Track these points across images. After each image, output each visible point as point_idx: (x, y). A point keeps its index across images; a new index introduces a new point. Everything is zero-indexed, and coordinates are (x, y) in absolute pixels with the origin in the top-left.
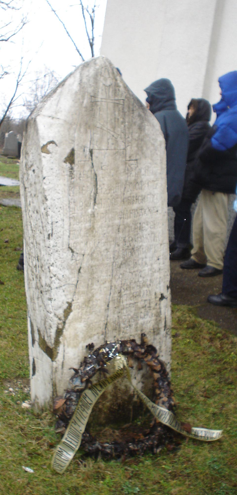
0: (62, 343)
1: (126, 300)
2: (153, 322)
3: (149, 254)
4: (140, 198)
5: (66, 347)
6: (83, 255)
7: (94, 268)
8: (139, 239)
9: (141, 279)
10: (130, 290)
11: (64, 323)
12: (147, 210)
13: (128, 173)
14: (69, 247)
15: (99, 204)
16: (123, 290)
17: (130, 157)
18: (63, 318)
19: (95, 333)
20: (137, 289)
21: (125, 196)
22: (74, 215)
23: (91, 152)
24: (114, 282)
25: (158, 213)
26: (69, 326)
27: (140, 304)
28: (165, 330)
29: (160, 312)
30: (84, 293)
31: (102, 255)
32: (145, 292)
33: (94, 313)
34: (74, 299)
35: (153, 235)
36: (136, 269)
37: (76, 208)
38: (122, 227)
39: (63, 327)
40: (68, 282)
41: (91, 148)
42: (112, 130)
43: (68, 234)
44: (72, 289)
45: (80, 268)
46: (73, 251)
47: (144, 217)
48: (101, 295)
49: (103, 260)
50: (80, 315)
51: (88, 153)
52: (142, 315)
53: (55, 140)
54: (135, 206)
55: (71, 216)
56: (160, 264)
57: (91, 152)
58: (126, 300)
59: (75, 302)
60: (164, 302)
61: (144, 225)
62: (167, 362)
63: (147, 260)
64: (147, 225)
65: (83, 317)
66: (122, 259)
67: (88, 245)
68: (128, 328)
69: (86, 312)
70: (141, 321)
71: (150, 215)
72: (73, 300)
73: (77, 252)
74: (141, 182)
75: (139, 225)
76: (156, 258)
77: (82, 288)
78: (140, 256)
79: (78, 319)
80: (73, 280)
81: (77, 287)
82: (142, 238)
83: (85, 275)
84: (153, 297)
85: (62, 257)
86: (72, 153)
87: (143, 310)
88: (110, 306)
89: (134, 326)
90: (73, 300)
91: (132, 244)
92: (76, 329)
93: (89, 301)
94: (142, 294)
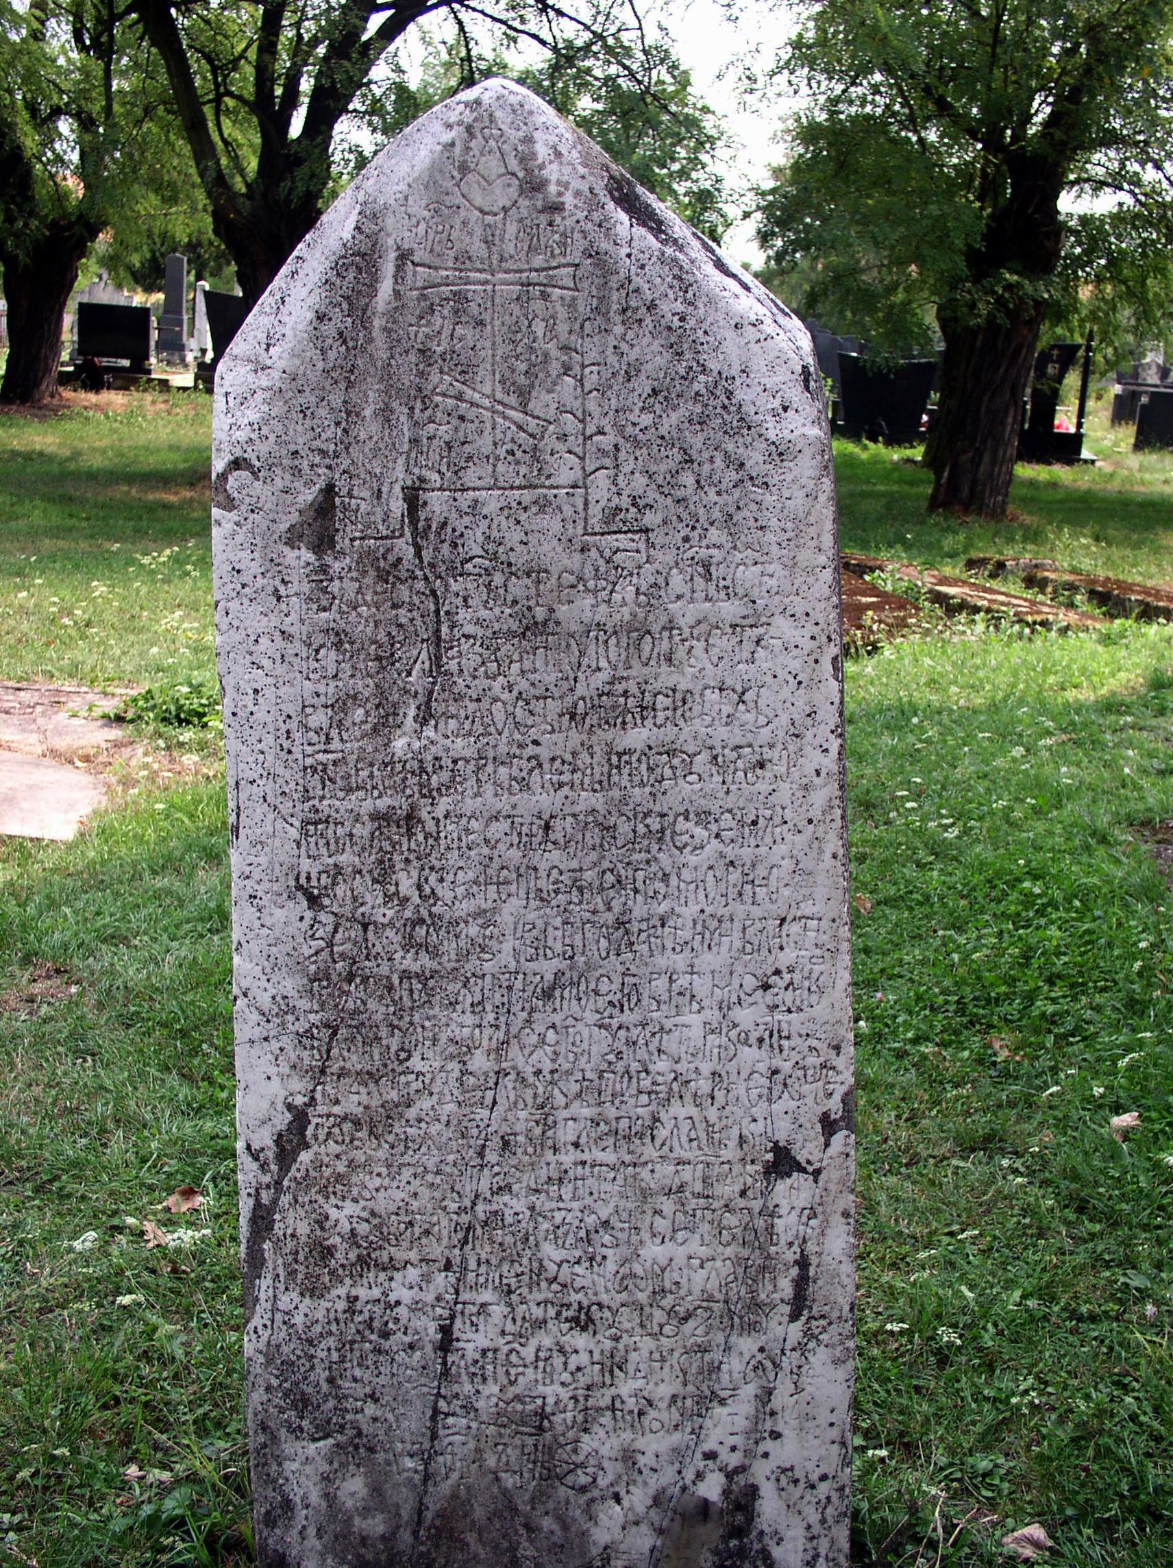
12: (702, 760)
28: (794, 1317)
29: (218, 978)
32: (685, 1126)
35: (735, 876)
54: (637, 737)
60: (792, 1194)
63: (701, 985)
66: (557, 964)
68: (578, 1269)
87: (668, 1206)
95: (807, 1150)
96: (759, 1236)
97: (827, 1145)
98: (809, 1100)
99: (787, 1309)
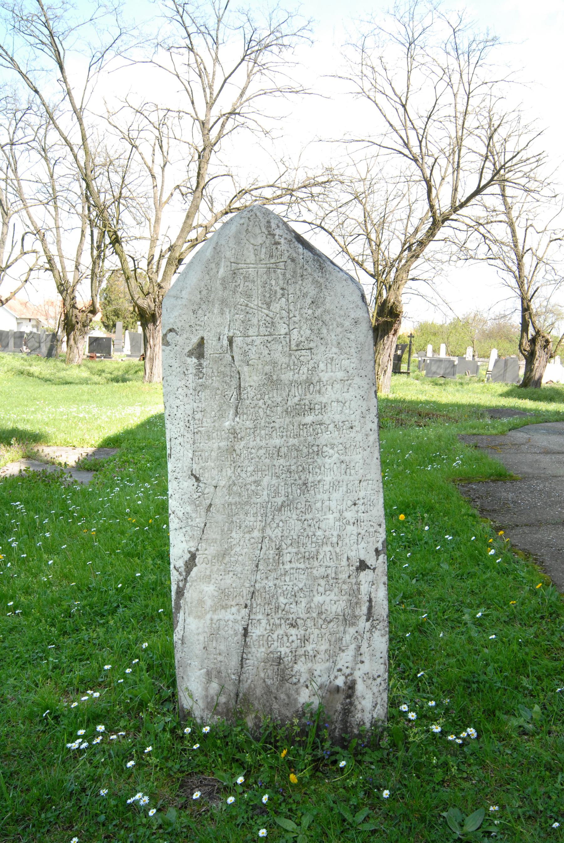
0: (183, 608)
1: (290, 562)
2: (342, 604)
3: (336, 496)
4: (317, 407)
5: (187, 614)
6: (216, 487)
7: (234, 507)
8: (317, 470)
9: (319, 533)
10: (298, 547)
11: (186, 579)
12: (331, 427)
13: (294, 370)
14: (192, 474)
15: (243, 414)
16: (284, 546)
17: (297, 345)
18: (184, 574)
19: (233, 603)
20: (311, 548)
21: (289, 403)
22: (200, 429)
23: (231, 341)
24: (268, 532)
25: (354, 430)
26: (190, 586)
27: (319, 572)
28: (368, 620)
30: (216, 542)
31: (247, 490)
33: (231, 574)
34: (199, 548)
35: (344, 466)
36: (308, 516)
37: (205, 420)
38: (284, 450)
39: (185, 585)
40: (190, 523)
41: (231, 334)
42: (265, 306)
43: (190, 455)
44: (198, 533)
45: (211, 505)
46: (197, 479)
47: (324, 438)
48: (243, 548)
49: (249, 497)
50: (208, 573)
51: (225, 342)
52: (321, 589)
53: (176, 328)
54: (309, 419)
55: (196, 430)
56: (357, 512)
57: (231, 341)
58: (290, 562)
59: (200, 552)
60: (365, 576)
61: (325, 449)
62: (400, 332)
63: (333, 504)
64: (332, 448)
65: (212, 576)
67: (224, 473)
69: (218, 569)
70: (318, 599)
71: (337, 433)
72: (197, 550)
73: (205, 481)
74: (319, 381)
75: (315, 449)
76: (350, 503)
77: (212, 534)
78: (319, 497)
79: (208, 578)
80: (199, 521)
81: (205, 532)
82: (322, 468)
83: (219, 517)
84: (344, 562)
85: (181, 487)
86: (201, 343)
87: (323, 582)
88: (260, 567)
89: (303, 604)
90: (197, 550)
91: (303, 477)
92: (201, 592)
93: (224, 554)
94: (320, 557)
95: (371, 560)
96: (355, 592)
97: (377, 559)
98: (371, 544)
99: (365, 617)
